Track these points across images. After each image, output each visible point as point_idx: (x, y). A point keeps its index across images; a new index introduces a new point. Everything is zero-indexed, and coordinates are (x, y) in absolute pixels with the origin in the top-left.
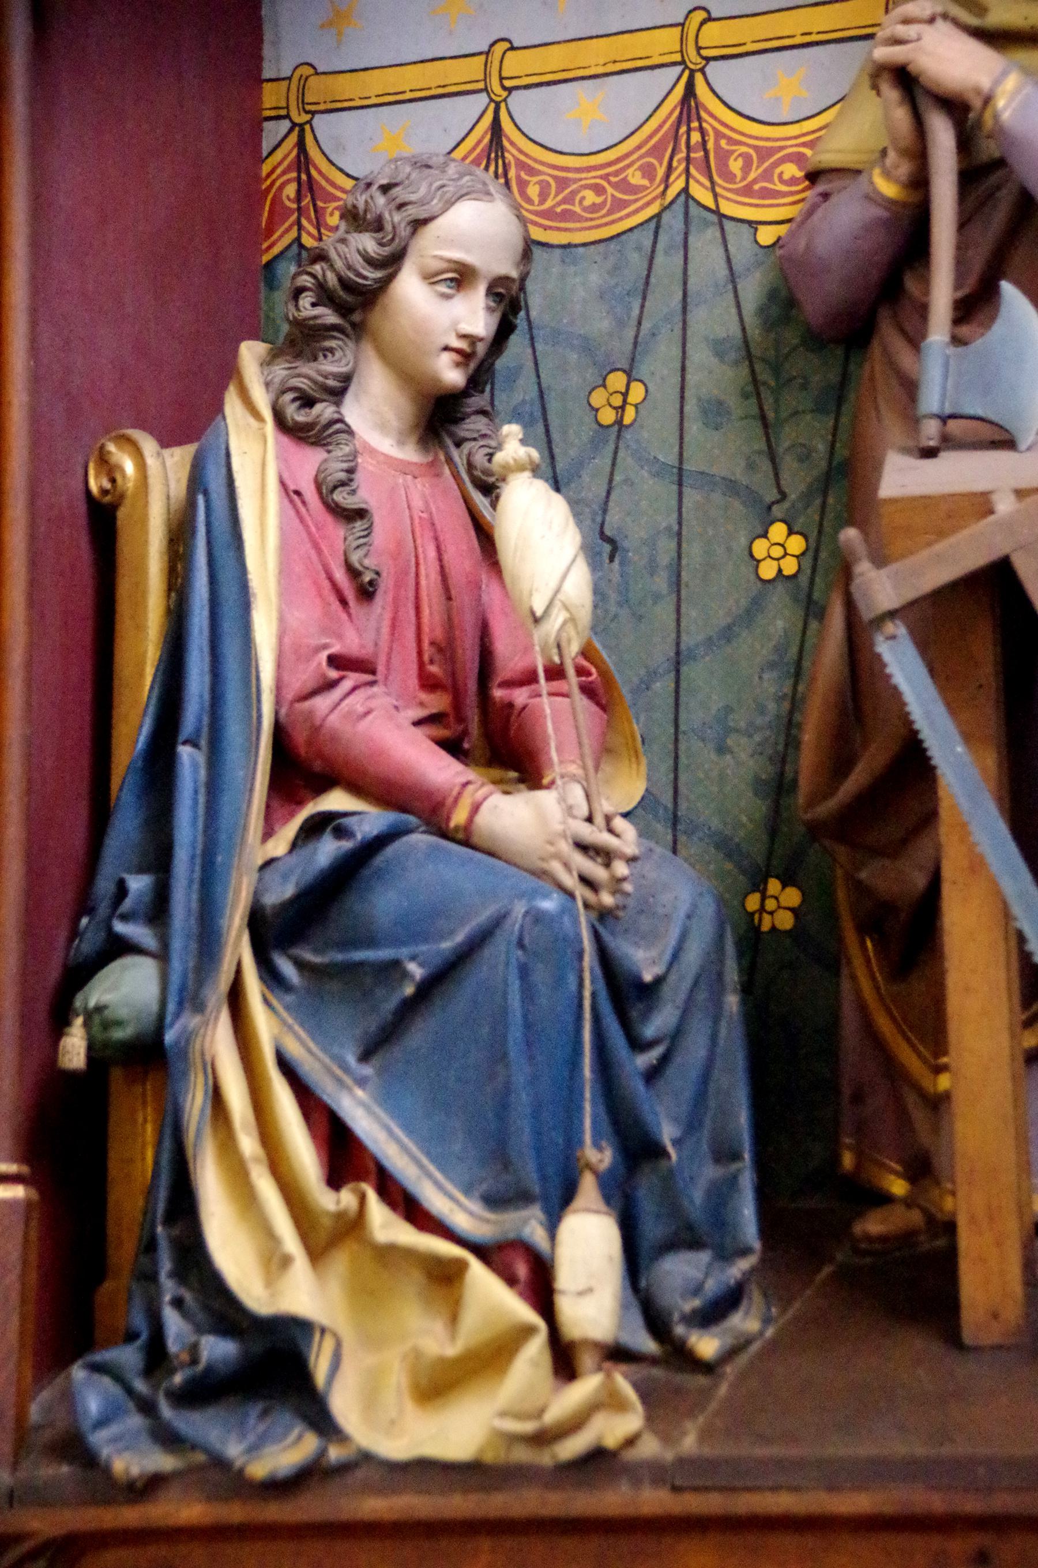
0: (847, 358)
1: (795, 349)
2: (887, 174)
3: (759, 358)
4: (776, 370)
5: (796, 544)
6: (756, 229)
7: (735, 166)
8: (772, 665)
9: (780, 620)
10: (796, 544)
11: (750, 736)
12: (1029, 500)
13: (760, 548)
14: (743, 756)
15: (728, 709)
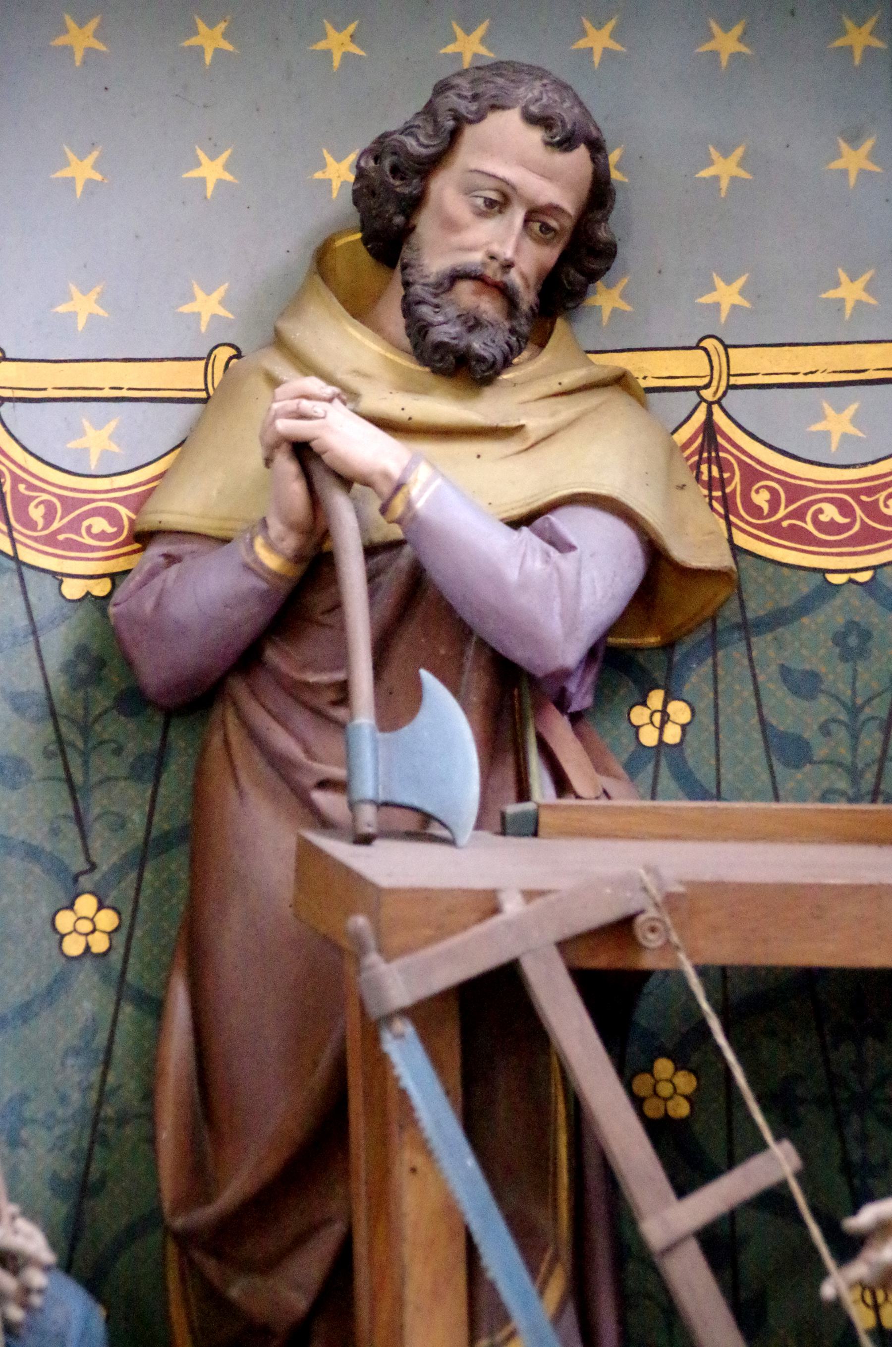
0: (166, 727)
1: (106, 712)
2: (271, 546)
3: (66, 717)
4: (85, 730)
5: (107, 920)
6: (61, 582)
7: (36, 513)
8: (77, 1052)
9: (88, 1001)
10: (107, 920)
11: (49, 1128)
12: (539, 902)
13: (65, 921)
14: (41, 1151)
15: (24, 1098)
